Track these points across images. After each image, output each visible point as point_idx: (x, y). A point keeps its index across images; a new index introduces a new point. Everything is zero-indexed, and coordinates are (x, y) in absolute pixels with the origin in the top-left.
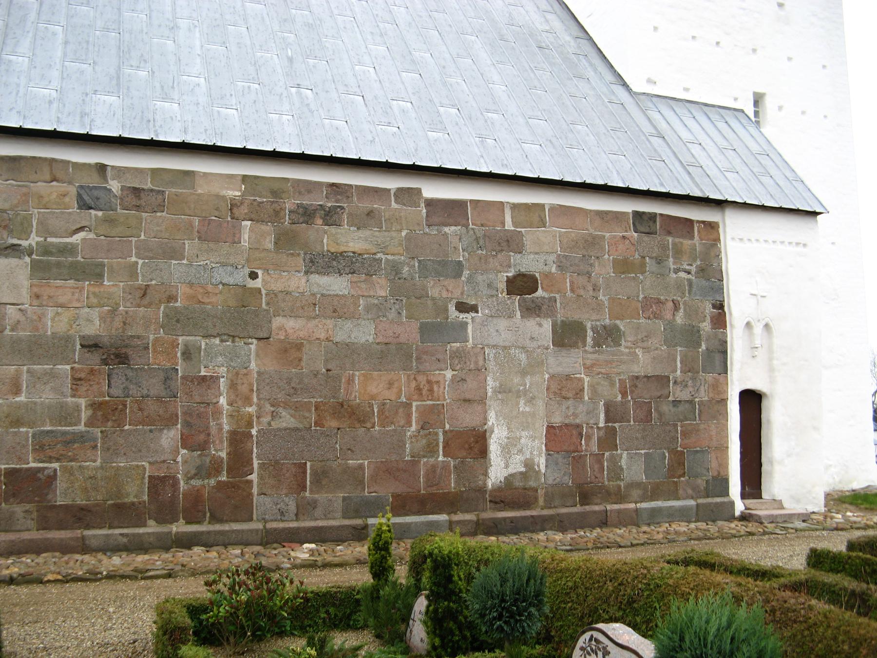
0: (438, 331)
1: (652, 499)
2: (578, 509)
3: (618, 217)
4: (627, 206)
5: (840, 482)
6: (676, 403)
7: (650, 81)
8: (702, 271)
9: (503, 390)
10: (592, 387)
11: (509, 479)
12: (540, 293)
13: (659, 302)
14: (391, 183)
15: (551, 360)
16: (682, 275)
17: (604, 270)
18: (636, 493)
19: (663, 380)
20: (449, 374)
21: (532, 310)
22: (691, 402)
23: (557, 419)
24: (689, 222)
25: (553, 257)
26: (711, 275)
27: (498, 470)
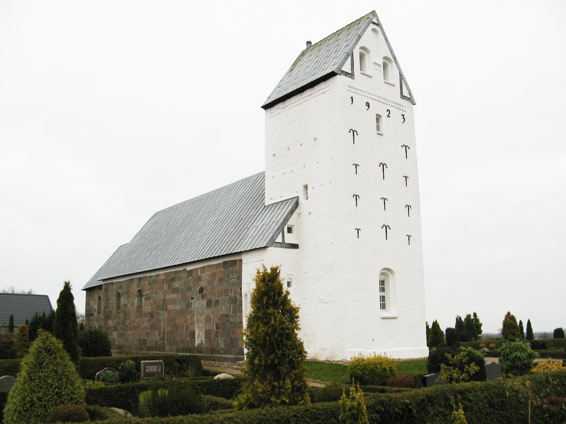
0: (189, 305)
1: (226, 354)
2: (211, 355)
3: (218, 265)
4: (221, 261)
5: (331, 357)
6: (231, 323)
7: (271, 199)
8: (238, 277)
9: (197, 320)
10: (213, 318)
11: (199, 344)
12: (204, 292)
13: (228, 290)
14: (181, 269)
15: (205, 312)
16: (233, 280)
17: (216, 282)
18: (222, 352)
19: (227, 316)
20: (189, 316)
21: (203, 297)
22: (234, 323)
23: (207, 328)
24: (236, 261)
25: (206, 281)
26: (86, 311)
27: (197, 343)
